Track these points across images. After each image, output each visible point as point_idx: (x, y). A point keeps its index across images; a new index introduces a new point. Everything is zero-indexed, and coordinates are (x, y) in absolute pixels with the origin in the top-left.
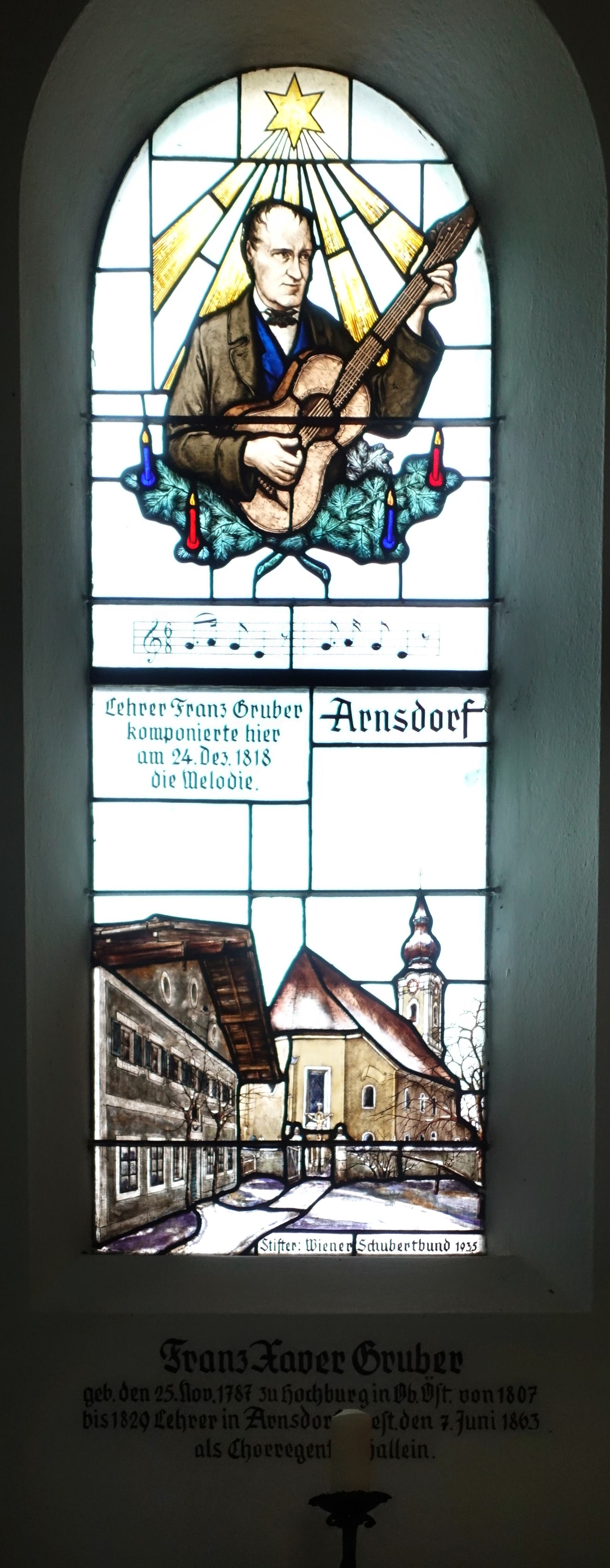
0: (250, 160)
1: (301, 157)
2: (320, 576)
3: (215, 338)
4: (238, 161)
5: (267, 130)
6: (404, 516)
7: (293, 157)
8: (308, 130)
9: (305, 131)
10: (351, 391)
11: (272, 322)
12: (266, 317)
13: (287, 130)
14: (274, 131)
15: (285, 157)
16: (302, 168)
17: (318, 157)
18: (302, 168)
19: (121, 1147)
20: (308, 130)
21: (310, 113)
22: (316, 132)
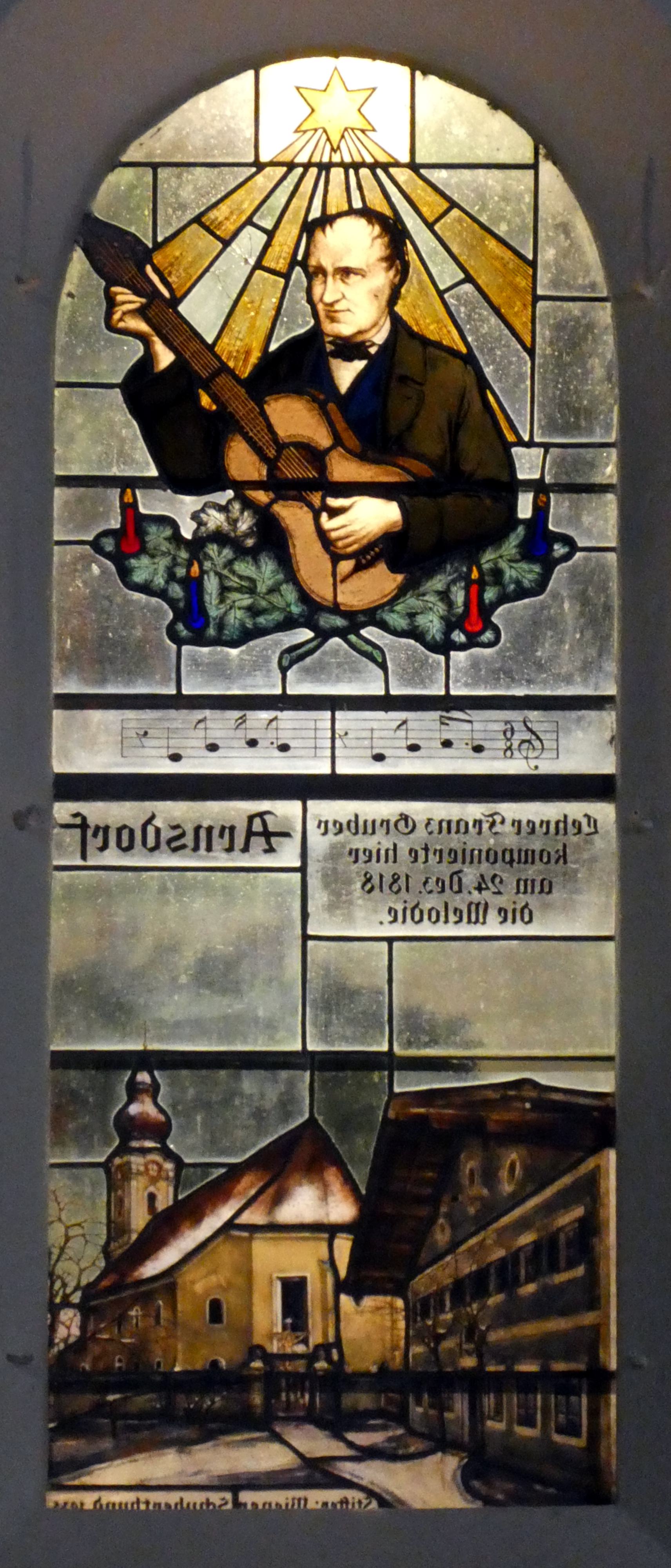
0: (273, 164)
1: (347, 159)
2: (373, 660)
3: (507, 375)
4: (259, 166)
5: (296, 131)
6: (490, 594)
7: (336, 158)
8: (353, 129)
9: (350, 131)
10: (247, 433)
11: (336, 354)
12: (329, 348)
13: (325, 131)
14: (305, 132)
15: (326, 159)
16: (324, 173)
17: (369, 160)
18: (324, 173)
19: (499, 1392)
20: (353, 129)
21: (313, 110)
22: (363, 131)
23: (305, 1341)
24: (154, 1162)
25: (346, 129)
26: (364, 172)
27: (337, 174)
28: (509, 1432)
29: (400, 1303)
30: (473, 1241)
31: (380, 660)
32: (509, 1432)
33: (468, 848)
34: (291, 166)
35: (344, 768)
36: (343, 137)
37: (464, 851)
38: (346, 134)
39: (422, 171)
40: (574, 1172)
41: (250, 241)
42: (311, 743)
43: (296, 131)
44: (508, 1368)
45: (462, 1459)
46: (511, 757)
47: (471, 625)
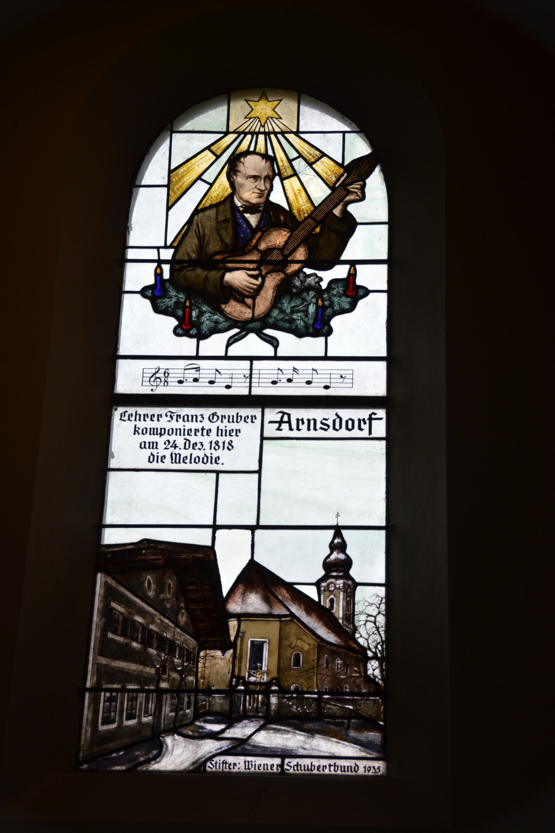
4: (227, 133)
7: (262, 130)
8: (272, 118)
14: (250, 118)
20: (272, 118)
22: (277, 118)
23: (250, 675)
24: (332, 583)
25: (268, 118)
26: (272, 136)
27: (261, 137)
28: (140, 722)
29: (202, 654)
30: (166, 621)
31: (230, 342)
32: (140, 722)
33: (228, 430)
34: (239, 134)
35: (256, 391)
36: (266, 122)
37: (184, 430)
38: (268, 121)
39: (286, 135)
40: (118, 585)
41: (300, 165)
42: (261, 380)
43: (245, 118)
44: (122, 686)
45: (163, 737)
46: (167, 386)
47: (185, 326)
